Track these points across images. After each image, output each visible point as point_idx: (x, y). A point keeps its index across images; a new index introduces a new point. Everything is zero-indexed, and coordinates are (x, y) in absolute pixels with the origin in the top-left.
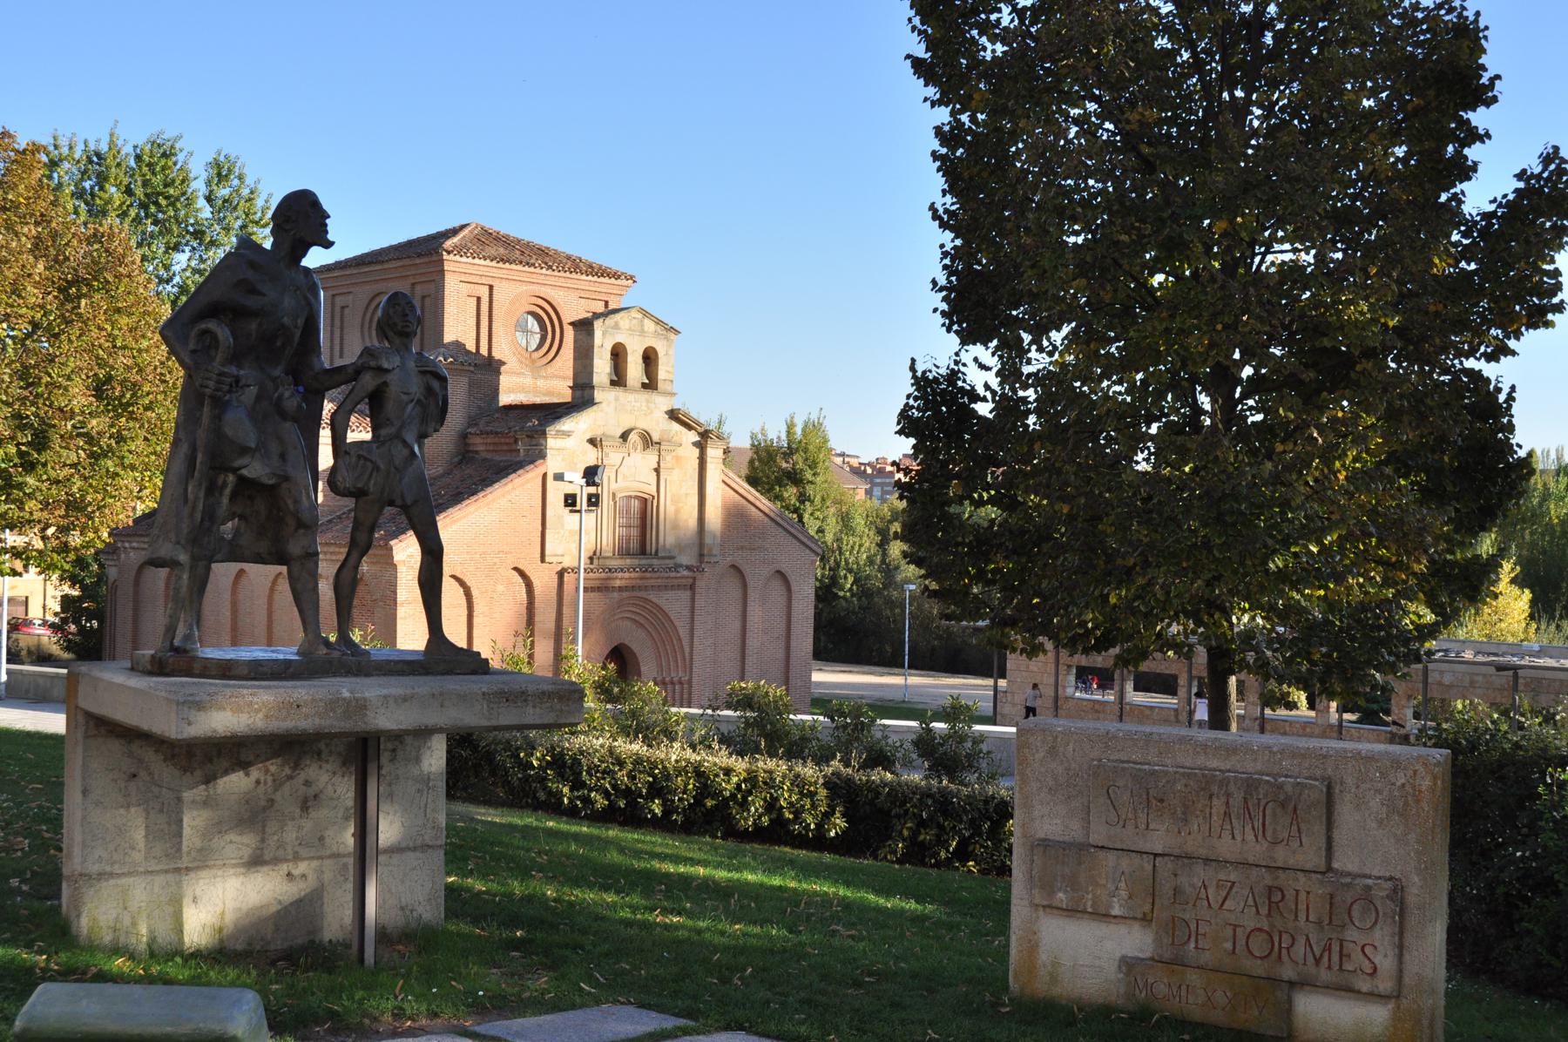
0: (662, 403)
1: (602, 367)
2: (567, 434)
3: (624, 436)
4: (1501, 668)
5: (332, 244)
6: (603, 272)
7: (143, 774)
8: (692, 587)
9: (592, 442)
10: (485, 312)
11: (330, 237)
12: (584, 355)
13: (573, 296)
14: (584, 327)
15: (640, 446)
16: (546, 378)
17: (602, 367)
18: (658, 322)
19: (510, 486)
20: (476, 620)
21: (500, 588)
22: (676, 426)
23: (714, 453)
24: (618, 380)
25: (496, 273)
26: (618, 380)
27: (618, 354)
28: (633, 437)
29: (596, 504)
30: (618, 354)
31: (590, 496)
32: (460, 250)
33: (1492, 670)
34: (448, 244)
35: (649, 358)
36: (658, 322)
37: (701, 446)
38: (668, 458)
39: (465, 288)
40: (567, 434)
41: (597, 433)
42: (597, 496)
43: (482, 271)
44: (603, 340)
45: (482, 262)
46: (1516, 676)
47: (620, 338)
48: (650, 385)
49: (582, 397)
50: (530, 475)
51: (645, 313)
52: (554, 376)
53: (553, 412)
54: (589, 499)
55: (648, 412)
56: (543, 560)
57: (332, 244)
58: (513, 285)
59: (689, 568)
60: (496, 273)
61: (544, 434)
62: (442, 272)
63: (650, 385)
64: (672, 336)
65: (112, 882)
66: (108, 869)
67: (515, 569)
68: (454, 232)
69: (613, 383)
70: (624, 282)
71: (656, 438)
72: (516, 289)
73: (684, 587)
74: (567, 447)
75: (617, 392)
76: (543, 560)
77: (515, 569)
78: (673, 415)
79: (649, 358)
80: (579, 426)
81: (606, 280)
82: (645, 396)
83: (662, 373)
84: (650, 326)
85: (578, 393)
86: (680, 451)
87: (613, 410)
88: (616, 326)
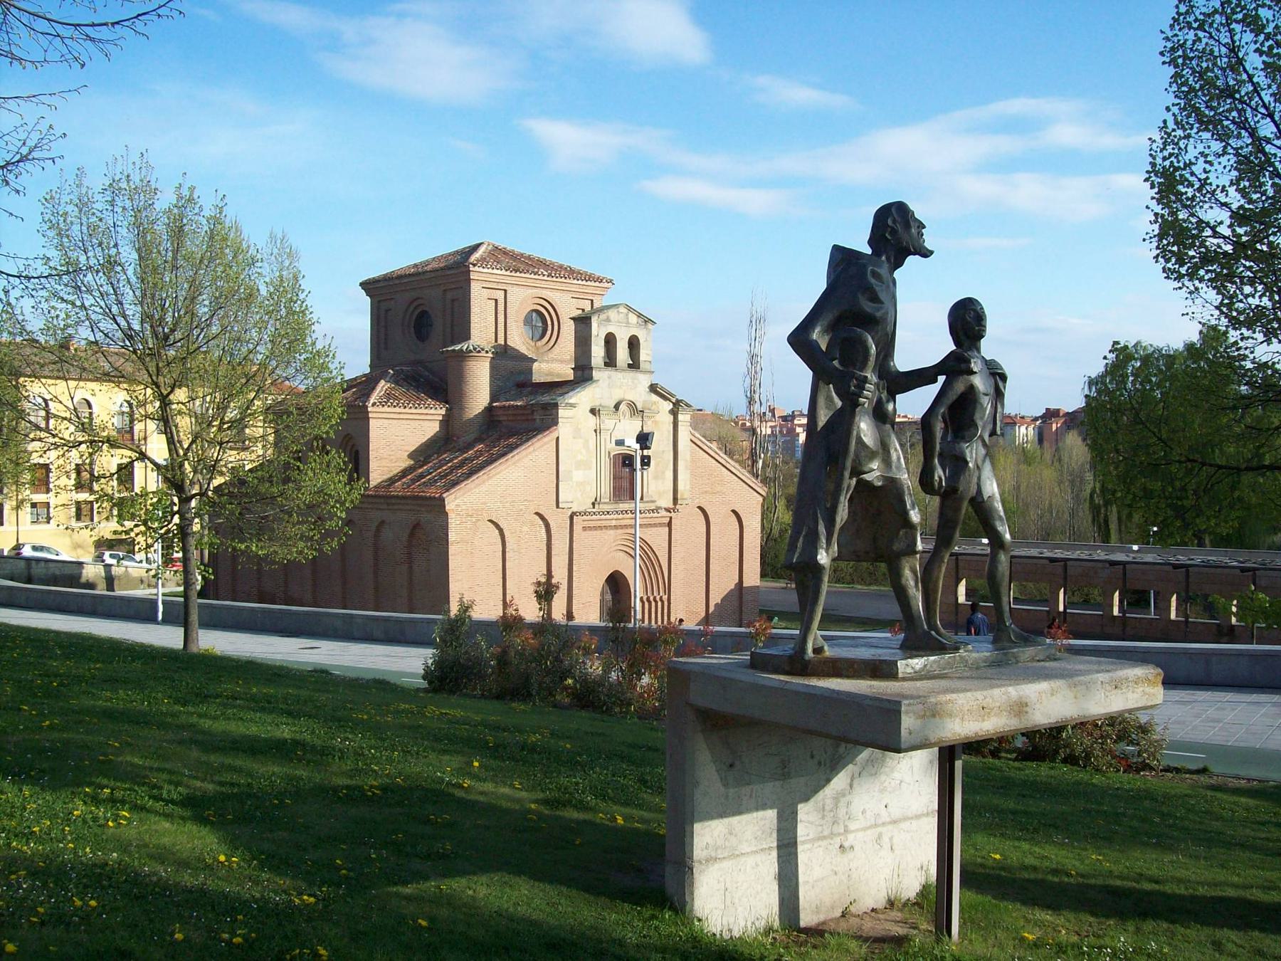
0: (644, 381)
1: (598, 352)
2: (573, 406)
3: (617, 407)
4: (1176, 567)
5: (932, 253)
6: (590, 278)
7: (737, 763)
8: (670, 524)
9: (593, 411)
10: (501, 309)
11: (928, 245)
12: (583, 342)
13: (568, 296)
14: (583, 322)
15: (628, 414)
16: (547, 362)
17: (598, 352)
18: (640, 315)
19: (531, 449)
20: (508, 555)
21: (525, 529)
22: (654, 397)
23: (684, 418)
24: (610, 361)
25: (509, 280)
26: (610, 361)
27: (610, 341)
28: (623, 407)
29: (648, 464)
30: (610, 341)
31: (643, 458)
32: (483, 261)
33: (1238, 571)
34: (473, 259)
35: (634, 344)
36: (640, 315)
37: (674, 413)
38: (649, 423)
39: (486, 293)
40: (573, 406)
41: (596, 404)
42: (649, 457)
43: (500, 279)
44: (598, 332)
45: (499, 272)
46: (1187, 571)
47: (611, 329)
48: (634, 365)
49: (583, 374)
50: (546, 440)
51: (630, 309)
52: (553, 360)
53: (560, 387)
54: (642, 460)
55: (634, 387)
56: (558, 506)
57: (932, 253)
58: (522, 289)
59: (668, 510)
60: (509, 280)
61: (556, 406)
62: (468, 280)
63: (634, 365)
64: (650, 326)
65: (717, 866)
66: (713, 854)
67: (537, 514)
68: (475, 248)
69: (606, 364)
70: (606, 285)
71: (640, 408)
72: (523, 294)
73: (661, 525)
74: (574, 413)
75: (609, 372)
76: (558, 506)
77: (537, 514)
78: (653, 389)
79: (634, 344)
80: (583, 398)
81: (592, 284)
82: (632, 374)
83: (644, 355)
84: (633, 318)
85: (579, 373)
86: (658, 417)
87: (607, 386)
88: (608, 320)
